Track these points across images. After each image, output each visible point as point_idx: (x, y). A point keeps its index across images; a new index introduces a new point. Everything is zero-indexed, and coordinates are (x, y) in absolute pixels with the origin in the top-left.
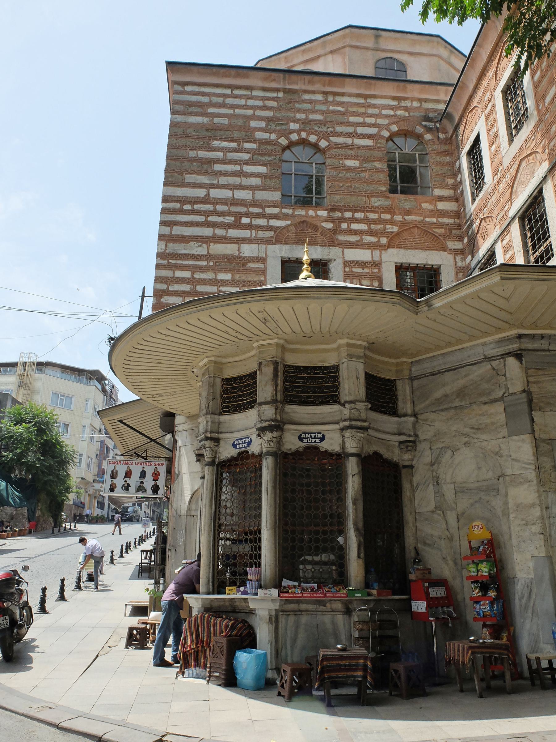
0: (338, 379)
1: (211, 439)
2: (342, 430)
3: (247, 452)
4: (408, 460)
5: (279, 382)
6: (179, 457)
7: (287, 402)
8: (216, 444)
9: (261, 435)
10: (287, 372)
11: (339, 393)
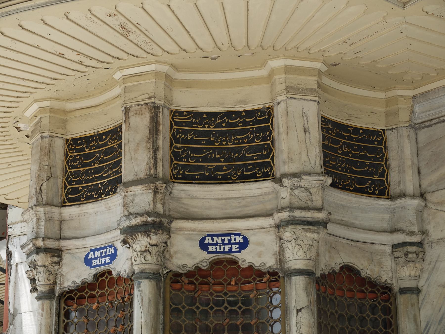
0: (271, 133)
1: (46, 250)
2: (278, 226)
3: (110, 272)
4: (410, 278)
5: (160, 143)
6: (15, 283)
7: (177, 178)
8: (55, 259)
9: (130, 241)
10: (177, 124)
11: (272, 158)
